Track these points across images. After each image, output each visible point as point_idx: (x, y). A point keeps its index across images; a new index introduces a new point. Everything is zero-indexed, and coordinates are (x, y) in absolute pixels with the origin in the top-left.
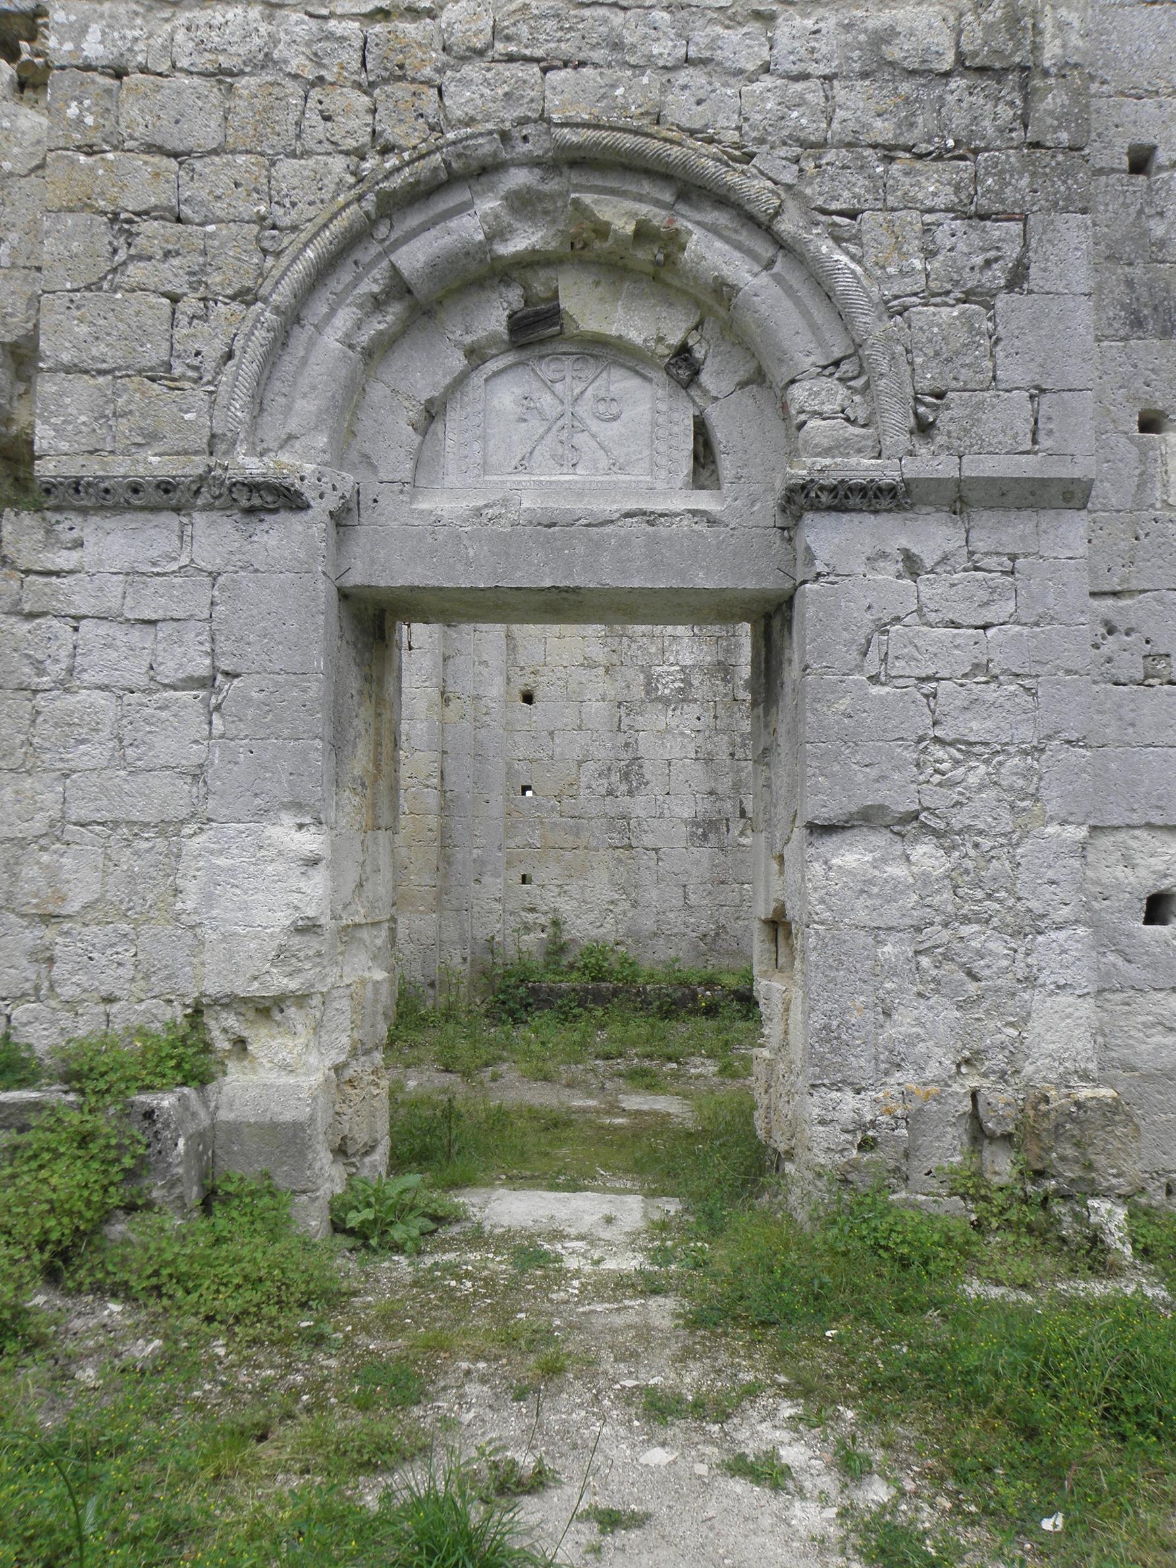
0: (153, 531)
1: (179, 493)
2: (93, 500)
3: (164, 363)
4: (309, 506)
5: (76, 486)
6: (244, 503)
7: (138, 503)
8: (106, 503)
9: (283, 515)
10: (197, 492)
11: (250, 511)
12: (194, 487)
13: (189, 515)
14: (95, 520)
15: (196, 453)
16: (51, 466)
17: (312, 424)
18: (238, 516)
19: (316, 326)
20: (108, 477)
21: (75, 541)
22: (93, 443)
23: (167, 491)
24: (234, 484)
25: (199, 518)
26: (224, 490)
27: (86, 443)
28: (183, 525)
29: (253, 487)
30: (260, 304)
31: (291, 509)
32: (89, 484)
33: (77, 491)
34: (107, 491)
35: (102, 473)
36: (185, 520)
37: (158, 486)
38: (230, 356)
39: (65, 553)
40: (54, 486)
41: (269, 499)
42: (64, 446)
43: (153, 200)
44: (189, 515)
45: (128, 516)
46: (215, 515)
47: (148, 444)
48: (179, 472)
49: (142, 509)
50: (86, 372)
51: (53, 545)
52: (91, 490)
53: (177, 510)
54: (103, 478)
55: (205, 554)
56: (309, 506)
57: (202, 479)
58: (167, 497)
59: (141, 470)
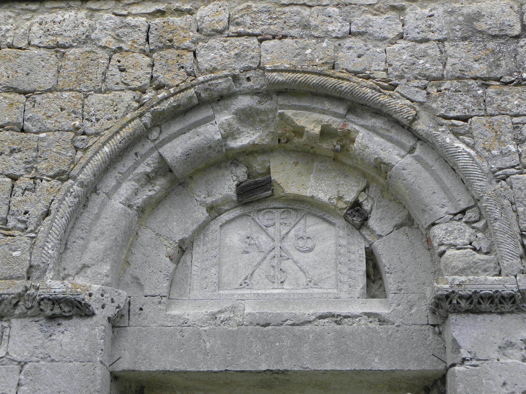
4: (94, 314)
6: (48, 312)
10: (16, 305)
11: (52, 318)
12: (14, 302)
13: (9, 320)
15: (18, 278)
19: (107, 194)
24: (42, 299)
26: (35, 304)
29: (55, 301)
31: (81, 316)
41: (66, 309)
43: (7, 119)
55: (17, 349)
56: (94, 314)
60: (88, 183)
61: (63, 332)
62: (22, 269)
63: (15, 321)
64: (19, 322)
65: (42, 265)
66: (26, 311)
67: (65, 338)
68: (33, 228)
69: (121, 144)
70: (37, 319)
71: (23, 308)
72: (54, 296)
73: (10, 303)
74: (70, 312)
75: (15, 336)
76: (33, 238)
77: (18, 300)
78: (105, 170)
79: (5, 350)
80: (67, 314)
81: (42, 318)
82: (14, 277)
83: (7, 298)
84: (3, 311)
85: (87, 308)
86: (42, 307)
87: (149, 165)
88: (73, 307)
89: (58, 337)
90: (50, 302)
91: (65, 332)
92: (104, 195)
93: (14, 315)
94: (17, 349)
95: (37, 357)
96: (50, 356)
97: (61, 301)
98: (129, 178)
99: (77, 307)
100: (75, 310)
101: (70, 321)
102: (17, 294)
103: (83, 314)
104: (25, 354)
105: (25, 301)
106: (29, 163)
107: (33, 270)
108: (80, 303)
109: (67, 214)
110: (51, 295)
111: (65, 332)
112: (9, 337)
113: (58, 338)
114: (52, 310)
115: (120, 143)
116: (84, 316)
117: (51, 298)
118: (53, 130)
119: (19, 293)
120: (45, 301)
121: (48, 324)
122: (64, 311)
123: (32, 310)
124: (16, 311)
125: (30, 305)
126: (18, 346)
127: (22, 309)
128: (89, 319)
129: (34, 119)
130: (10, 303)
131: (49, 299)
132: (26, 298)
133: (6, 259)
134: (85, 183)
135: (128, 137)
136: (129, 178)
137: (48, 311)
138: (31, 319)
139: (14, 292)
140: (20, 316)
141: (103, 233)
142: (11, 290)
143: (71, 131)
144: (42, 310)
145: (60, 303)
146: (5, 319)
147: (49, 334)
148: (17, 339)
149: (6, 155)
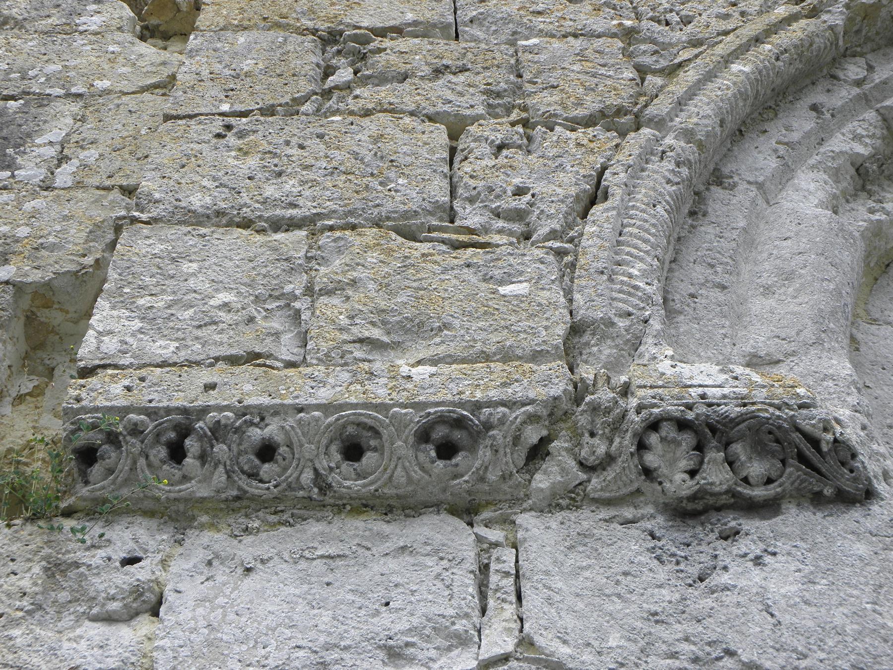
0: (392, 564)
1: (484, 454)
2: (219, 476)
3: (438, 206)
4: (869, 495)
5: (177, 437)
6: (678, 483)
7: (356, 485)
8: (254, 488)
9: (794, 519)
10: (538, 453)
11: (691, 511)
12: (532, 435)
13: (508, 522)
14: (204, 541)
15: (536, 356)
16: (117, 389)
17: (808, 334)
18: (658, 523)
19: (760, 186)
20: (277, 411)
21: (137, 591)
22: (248, 342)
23: (447, 450)
24: (654, 426)
25: (540, 533)
26: (625, 443)
27: (223, 342)
28: (486, 547)
29: (707, 431)
30: (646, 131)
31: (817, 500)
32: (218, 431)
33: (177, 453)
34: (267, 451)
35: (265, 400)
36: (495, 534)
37: (424, 436)
38: (596, 195)
39: (95, 631)
40: (113, 439)
41: (756, 468)
42: (163, 348)
43: (410, 16)
44: (508, 522)
45: (314, 528)
46: (587, 519)
47: (396, 346)
48: (494, 394)
49: (363, 506)
50: (246, 224)
51: (61, 608)
52: (220, 449)
53: (467, 511)
54: (262, 414)
55: (569, 621)
56: (869, 495)
57: (556, 414)
58: (451, 466)
59: (380, 391)
60: (708, 135)
61: (757, 561)
62: (546, 328)
63: (533, 521)
64: (554, 525)
65: (622, 323)
66: (583, 476)
67: (781, 580)
68: (556, 225)
69: (780, 63)
70: (628, 513)
71: (572, 463)
72: (702, 409)
73: (516, 440)
74: (769, 481)
75: (547, 573)
76: (560, 253)
77: (545, 433)
78: (734, 135)
79: (508, 630)
80: (759, 493)
81: (650, 510)
82: (519, 352)
83: (502, 421)
84: (482, 479)
85: (843, 464)
86: (651, 459)
87: (857, 138)
88: (783, 462)
89: (738, 575)
90: (687, 439)
91: (768, 559)
92: (753, 192)
93: (527, 496)
94: (569, 621)
95: (674, 655)
96: (730, 653)
97: (734, 433)
98: (812, 161)
99: (802, 458)
100: (794, 471)
101: (778, 519)
102: (545, 403)
103: (828, 491)
104: (612, 643)
105: (576, 435)
106: (498, 95)
107: (586, 338)
108: (815, 443)
109: (667, 198)
110: (690, 407)
111: (768, 559)
112: (517, 576)
113: (742, 583)
114: (692, 473)
115: (777, 59)
116: (830, 501)
117: (690, 416)
118: (559, 35)
119: (555, 399)
120: (668, 430)
121: (681, 537)
122: (746, 480)
123: (610, 474)
124: (538, 476)
125: (602, 449)
126: (572, 610)
127: (563, 471)
128: (856, 513)
129: (490, 19)
130: (516, 440)
131: (682, 425)
132: (583, 420)
133: (476, 301)
134: (700, 136)
135: (796, 46)
136: (812, 161)
137: (679, 477)
138: (604, 513)
139: (532, 395)
140: (553, 504)
141: (789, 276)
142: (517, 391)
143: (614, 36)
144: (648, 472)
145: (727, 445)
146: (486, 514)
147: (694, 571)
148: (560, 585)
149: (422, 78)
